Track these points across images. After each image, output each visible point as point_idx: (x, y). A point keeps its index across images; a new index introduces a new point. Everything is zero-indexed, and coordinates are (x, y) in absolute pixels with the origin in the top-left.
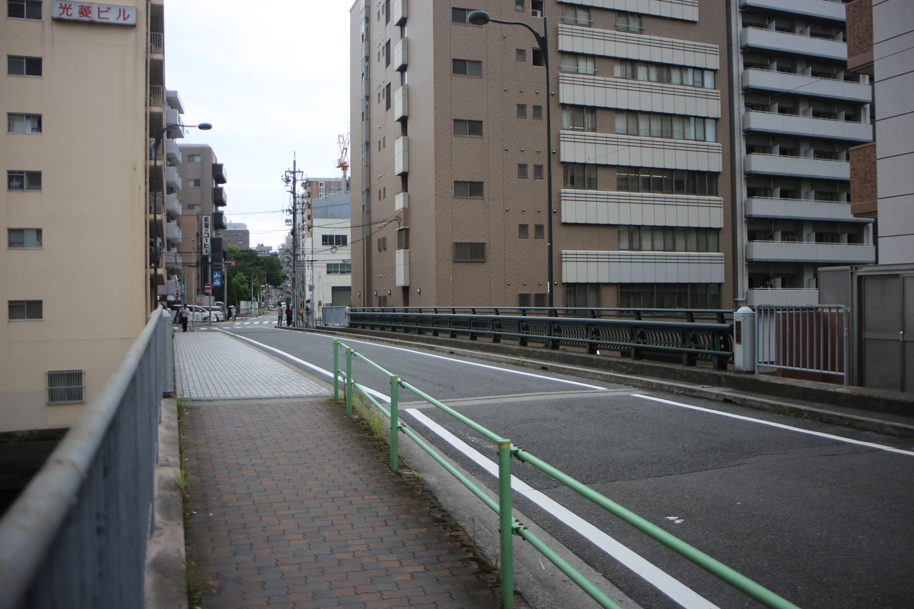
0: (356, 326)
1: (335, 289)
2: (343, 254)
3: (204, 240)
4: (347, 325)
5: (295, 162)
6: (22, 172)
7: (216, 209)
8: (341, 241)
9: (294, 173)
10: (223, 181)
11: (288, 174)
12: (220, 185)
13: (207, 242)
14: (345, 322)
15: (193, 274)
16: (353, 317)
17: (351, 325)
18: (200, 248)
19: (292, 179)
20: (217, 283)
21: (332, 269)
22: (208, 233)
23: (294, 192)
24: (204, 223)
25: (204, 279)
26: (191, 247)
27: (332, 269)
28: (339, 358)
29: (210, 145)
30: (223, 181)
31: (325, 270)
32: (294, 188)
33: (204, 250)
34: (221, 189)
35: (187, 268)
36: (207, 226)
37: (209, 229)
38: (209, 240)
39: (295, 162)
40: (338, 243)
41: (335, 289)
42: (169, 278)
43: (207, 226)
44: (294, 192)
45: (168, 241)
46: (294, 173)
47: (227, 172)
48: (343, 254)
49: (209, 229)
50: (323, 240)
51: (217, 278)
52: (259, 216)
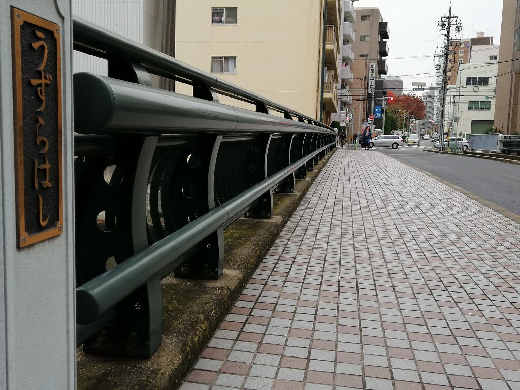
0: (509, 152)
1: (474, 122)
2: (482, 93)
3: (370, 83)
4: (498, 151)
5: (451, 8)
6: (222, 9)
7: (381, 59)
8: (484, 81)
9: (449, 18)
10: (386, 54)
11: (444, 19)
12: (383, 58)
13: (372, 84)
14: (498, 148)
15: (361, 105)
16: (505, 144)
17: (503, 151)
18: (366, 89)
19: (447, 24)
20: (378, 115)
21: (473, 105)
22: (373, 76)
23: (448, 35)
24: (370, 68)
25: (368, 112)
26: (360, 84)
27: (473, 105)
28: (235, 124)
29: (378, 7)
30: (386, 54)
31: (467, 105)
32: (449, 32)
33: (370, 90)
34: (385, 42)
35: (355, 101)
36: (372, 71)
37: (374, 73)
38: (374, 83)
39: (451, 8)
40: (480, 84)
41: (474, 122)
42: (342, 110)
43: (372, 71)
44: (448, 35)
45: (343, 80)
46: (449, 18)
47: (390, 29)
48: (482, 93)
49: (374, 73)
50: (467, 81)
51: (378, 111)
52: (412, 65)
